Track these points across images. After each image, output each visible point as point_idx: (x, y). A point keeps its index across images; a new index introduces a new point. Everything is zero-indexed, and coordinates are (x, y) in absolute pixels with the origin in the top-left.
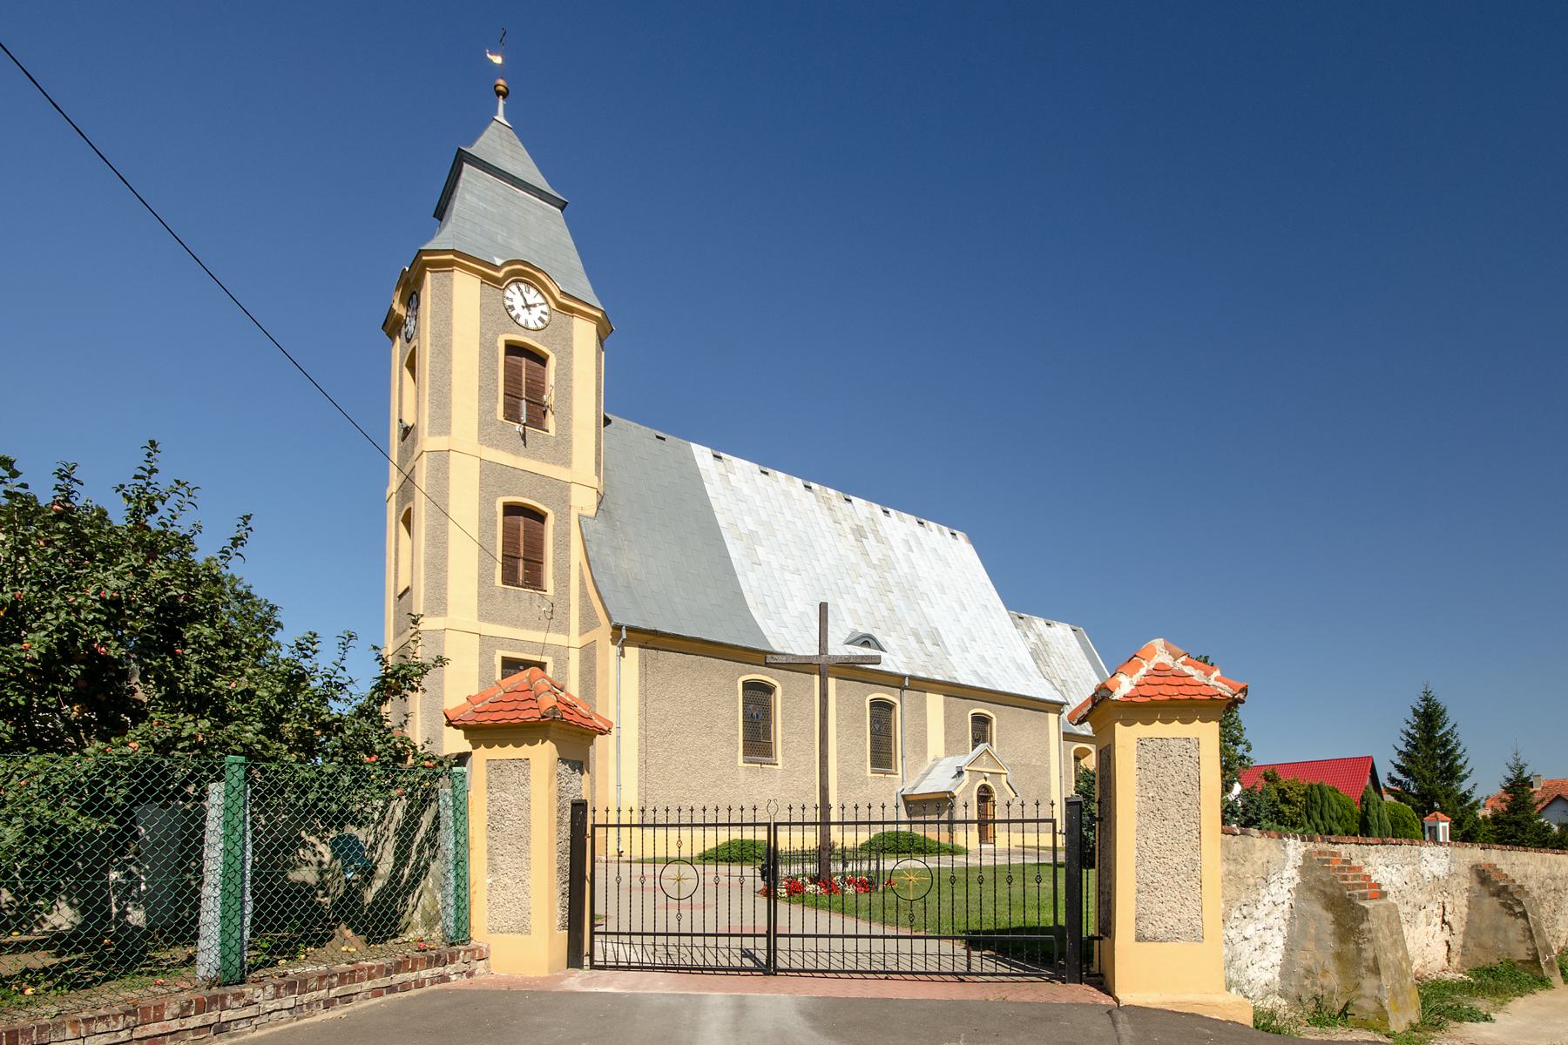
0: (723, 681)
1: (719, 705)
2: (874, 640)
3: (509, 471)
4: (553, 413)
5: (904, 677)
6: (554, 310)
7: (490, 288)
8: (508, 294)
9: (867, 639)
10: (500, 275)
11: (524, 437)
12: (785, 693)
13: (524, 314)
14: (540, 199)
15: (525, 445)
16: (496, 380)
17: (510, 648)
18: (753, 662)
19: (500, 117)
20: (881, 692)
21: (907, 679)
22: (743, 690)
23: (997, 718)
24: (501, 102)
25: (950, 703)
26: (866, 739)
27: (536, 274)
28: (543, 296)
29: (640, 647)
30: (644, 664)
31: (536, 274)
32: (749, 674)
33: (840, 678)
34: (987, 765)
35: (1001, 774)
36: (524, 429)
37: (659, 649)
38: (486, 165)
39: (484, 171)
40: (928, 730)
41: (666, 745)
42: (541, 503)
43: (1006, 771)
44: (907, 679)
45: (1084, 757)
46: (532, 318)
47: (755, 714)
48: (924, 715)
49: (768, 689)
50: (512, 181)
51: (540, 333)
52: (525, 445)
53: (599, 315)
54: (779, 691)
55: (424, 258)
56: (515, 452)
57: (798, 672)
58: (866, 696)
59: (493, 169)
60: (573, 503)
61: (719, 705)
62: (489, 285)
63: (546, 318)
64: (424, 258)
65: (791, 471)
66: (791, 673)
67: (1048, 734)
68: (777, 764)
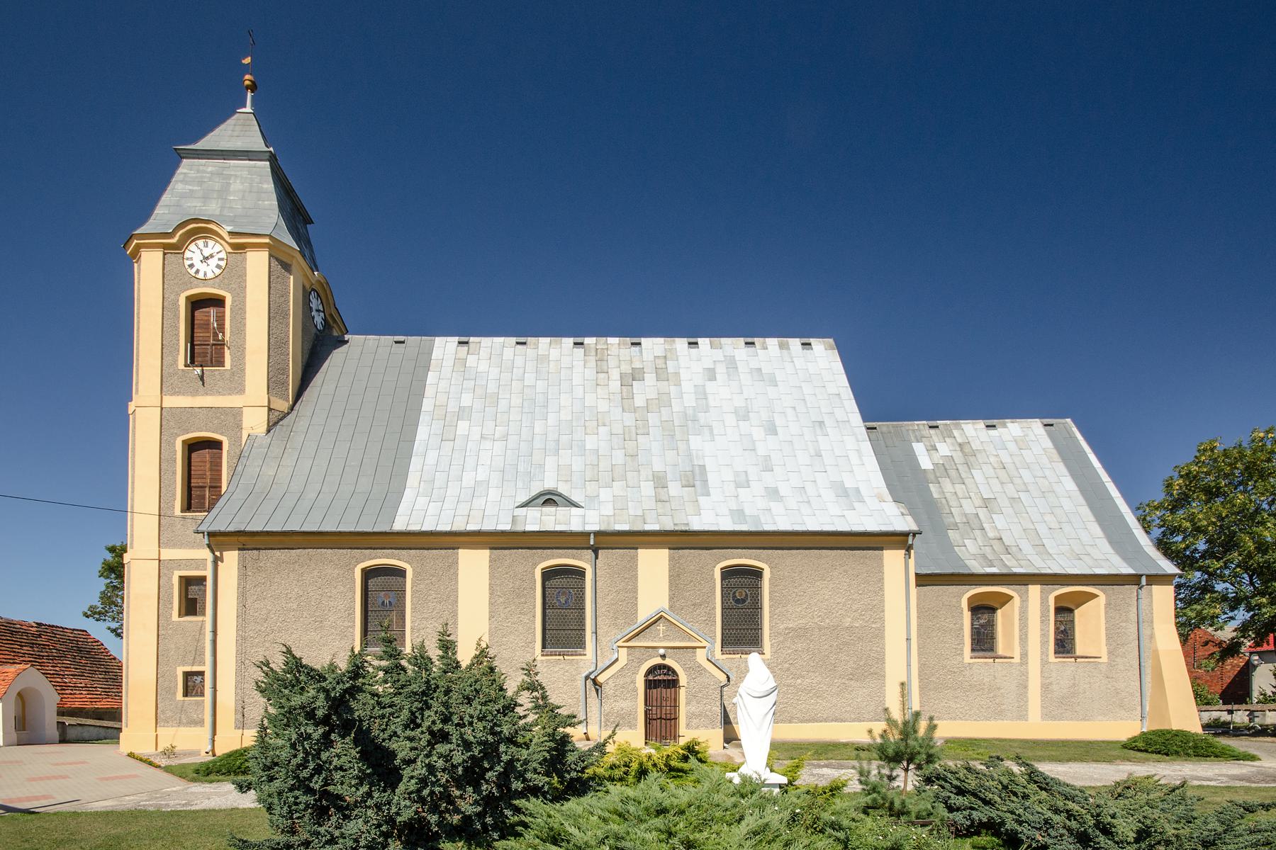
0: (336, 571)
1: (330, 597)
2: (560, 495)
3: (188, 412)
4: (229, 348)
5: (587, 534)
6: (229, 253)
7: (173, 255)
8: (188, 254)
9: (547, 497)
10: (174, 240)
11: (202, 378)
12: (416, 574)
13: (203, 267)
14: (250, 160)
15: (203, 384)
16: (178, 335)
17: (187, 568)
18: (373, 546)
19: (248, 109)
20: (553, 557)
21: (592, 536)
22: (722, 580)
23: (771, 568)
24: (249, 95)
25: (680, 558)
26: (534, 617)
27: (208, 226)
28: (221, 245)
29: (239, 549)
30: (243, 567)
31: (208, 226)
32: (370, 559)
33: (496, 549)
34: (666, 638)
35: (695, 648)
36: (203, 370)
37: (259, 549)
38: (224, 153)
39: (199, 159)
40: (639, 596)
41: (267, 645)
42: (217, 433)
43: (704, 643)
44: (592, 536)
45: (1003, 604)
46: (210, 270)
47: (387, 601)
48: (635, 577)
49: (757, 574)
50: (247, 156)
51: (217, 280)
52: (203, 384)
53: (267, 240)
54: (767, 575)
55: (128, 253)
56: (195, 393)
57: (436, 549)
58: (535, 565)
59: (205, 153)
60: (244, 426)
61: (330, 597)
62: (171, 253)
63: (223, 264)
64: (128, 253)
65: (555, 331)
66: (426, 551)
67: (881, 580)
68: (585, 655)
